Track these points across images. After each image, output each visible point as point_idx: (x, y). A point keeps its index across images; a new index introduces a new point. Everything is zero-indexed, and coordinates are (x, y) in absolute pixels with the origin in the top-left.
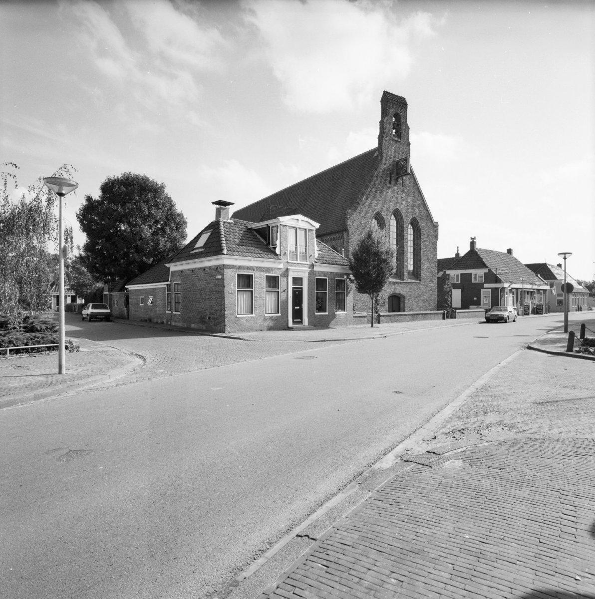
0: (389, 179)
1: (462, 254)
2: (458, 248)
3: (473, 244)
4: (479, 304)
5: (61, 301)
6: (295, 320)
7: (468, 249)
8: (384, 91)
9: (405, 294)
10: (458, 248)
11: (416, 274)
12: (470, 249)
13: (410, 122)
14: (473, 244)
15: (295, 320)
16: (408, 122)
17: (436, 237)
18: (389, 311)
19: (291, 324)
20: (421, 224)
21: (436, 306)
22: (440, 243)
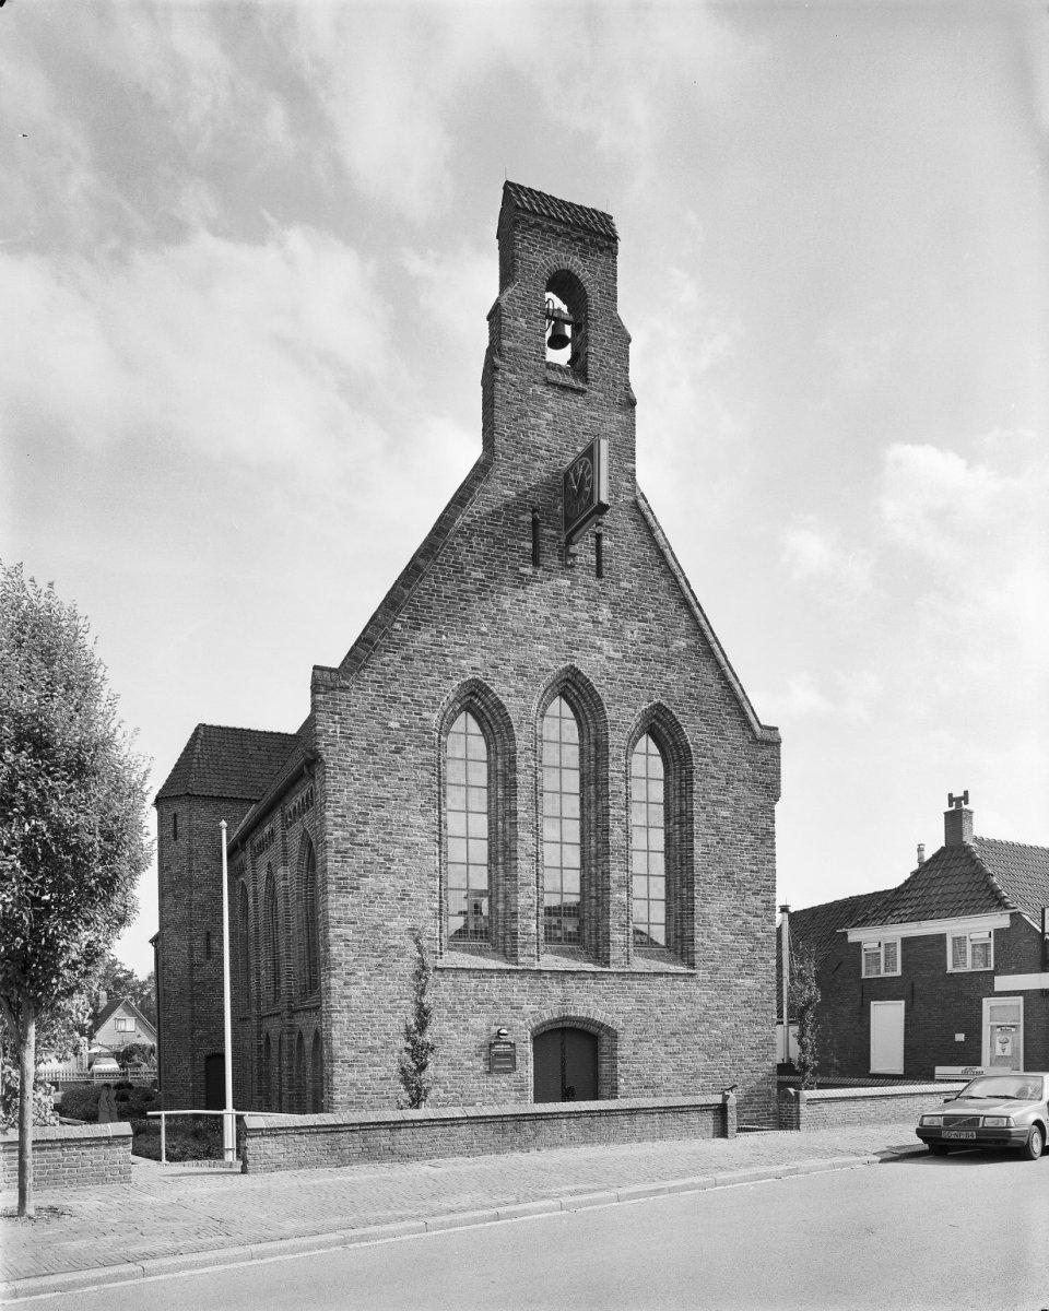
0: (529, 545)
3: (956, 818)
8: (507, 183)
14: (956, 818)
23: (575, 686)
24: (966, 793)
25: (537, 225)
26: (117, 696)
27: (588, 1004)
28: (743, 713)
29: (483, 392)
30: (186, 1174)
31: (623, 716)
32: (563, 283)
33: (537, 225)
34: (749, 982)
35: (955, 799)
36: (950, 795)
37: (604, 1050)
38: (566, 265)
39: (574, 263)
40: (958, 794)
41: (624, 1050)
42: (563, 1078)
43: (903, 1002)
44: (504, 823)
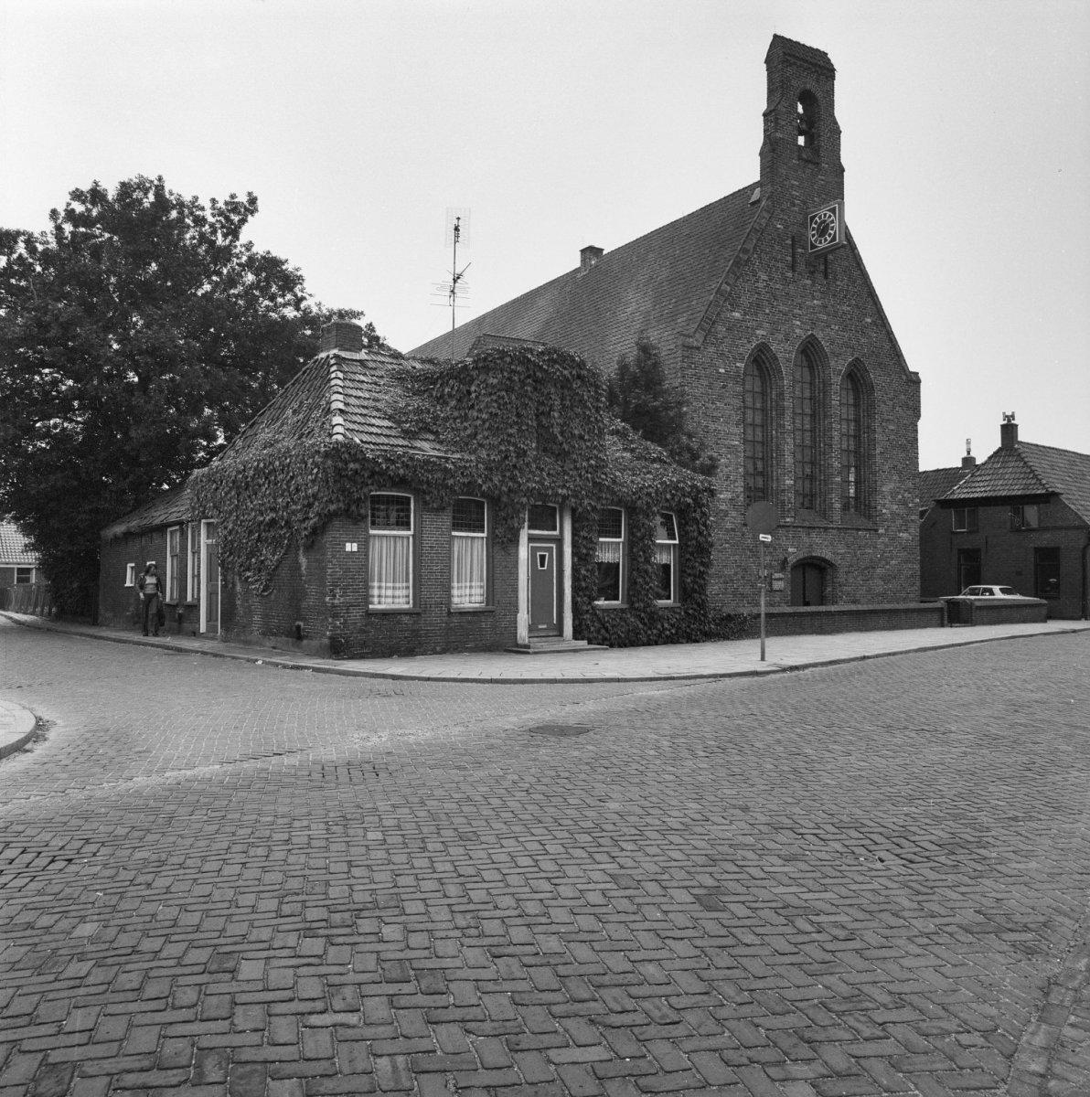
0: (789, 258)
1: (980, 459)
2: (968, 442)
3: (1009, 430)
4: (264, 634)
5: (474, 608)
6: (203, 628)
7: (995, 443)
8: (778, 41)
9: (837, 561)
10: (968, 442)
11: (863, 505)
12: (1002, 444)
13: (841, 113)
14: (1009, 430)
15: (203, 628)
16: (836, 115)
17: (916, 413)
18: (793, 604)
19: (556, 533)
20: (875, 376)
21: (918, 593)
22: (926, 429)
23: (812, 346)
24: (1013, 413)
25: (795, 63)
26: (371, 325)
27: (824, 548)
28: (480, 612)
29: (761, 160)
30: (304, 965)
31: (838, 366)
32: (807, 98)
33: (795, 63)
34: (904, 535)
35: (1007, 416)
36: (1004, 413)
37: (828, 577)
38: (808, 86)
39: (811, 85)
40: (1009, 413)
41: (841, 578)
42: (804, 594)
43: (921, 469)
44: (776, 432)
